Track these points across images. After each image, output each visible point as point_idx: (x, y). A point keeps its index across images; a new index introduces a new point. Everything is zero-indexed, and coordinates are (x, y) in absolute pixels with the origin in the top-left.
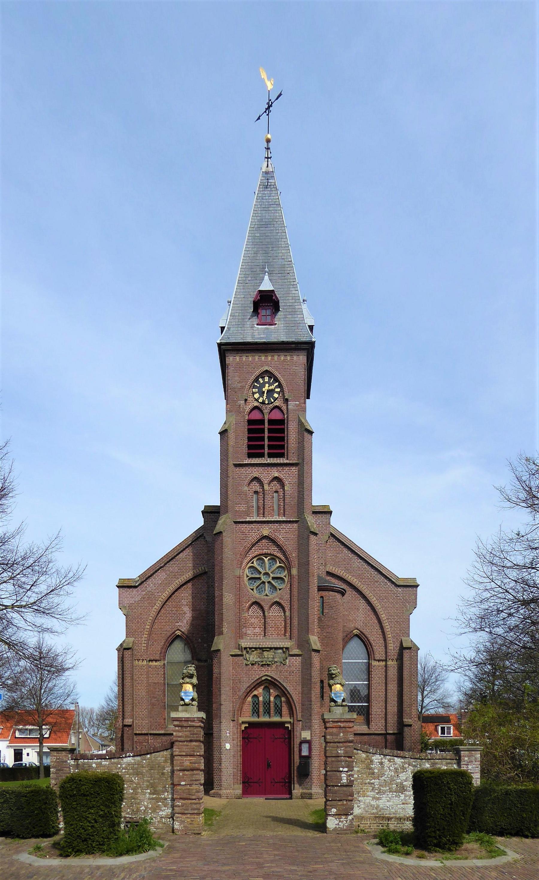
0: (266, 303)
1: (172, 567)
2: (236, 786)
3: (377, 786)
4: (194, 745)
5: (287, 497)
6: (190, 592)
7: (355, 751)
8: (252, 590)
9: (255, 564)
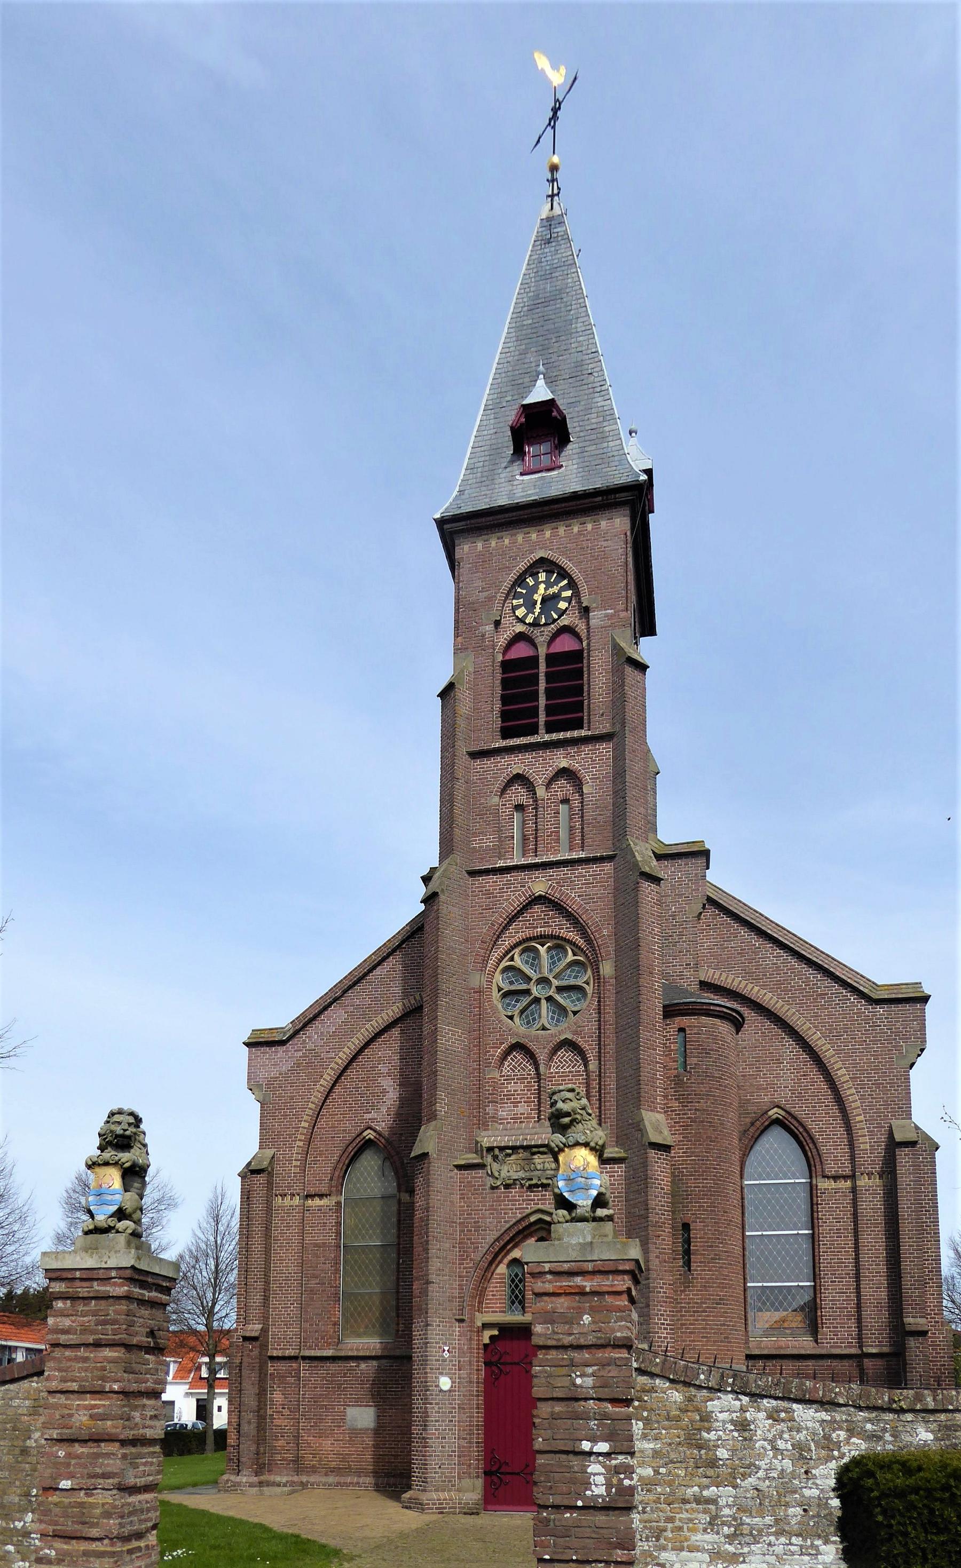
0: (540, 428)
1: (355, 998)
2: (467, 1482)
3: (726, 1511)
4: (107, 1359)
5: (589, 807)
6: (397, 1046)
7: (642, 1380)
8: (511, 1018)
9: (518, 962)
